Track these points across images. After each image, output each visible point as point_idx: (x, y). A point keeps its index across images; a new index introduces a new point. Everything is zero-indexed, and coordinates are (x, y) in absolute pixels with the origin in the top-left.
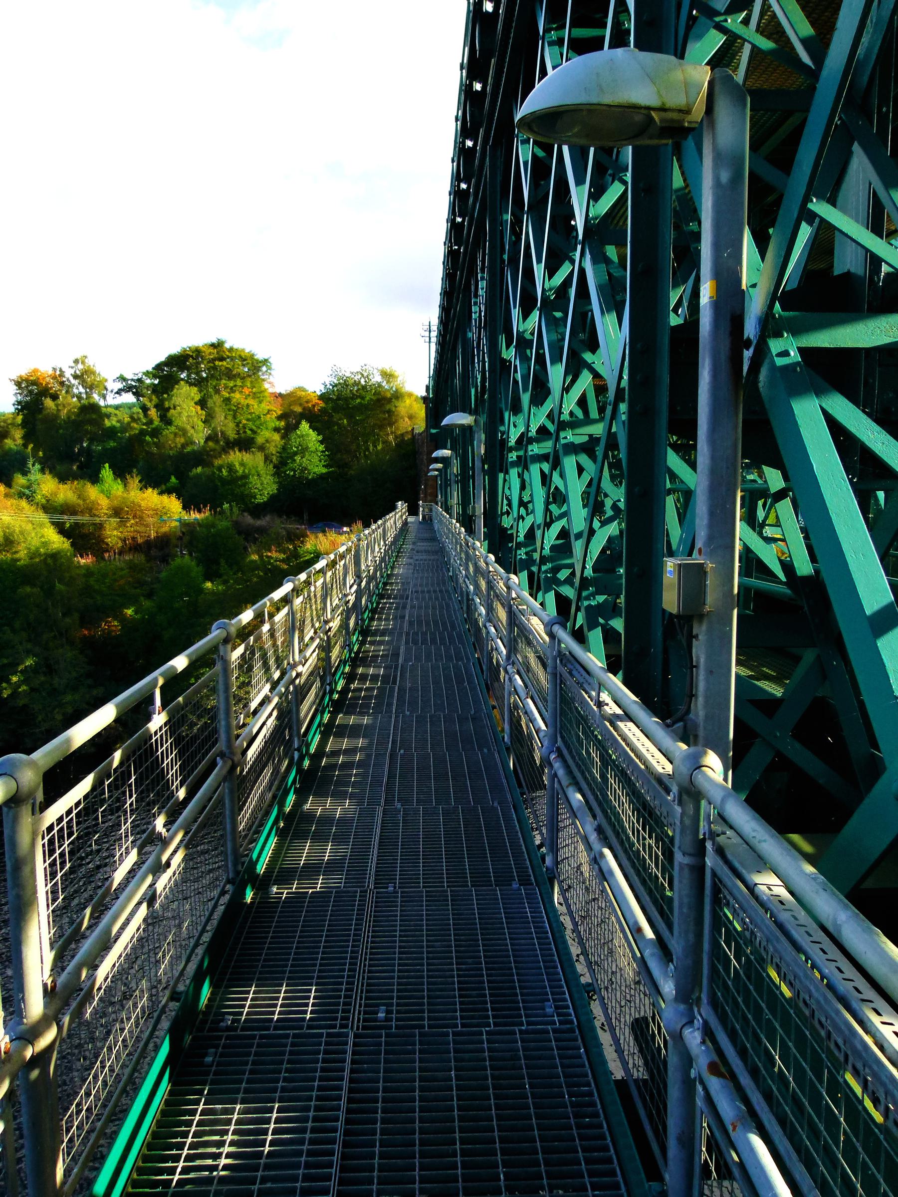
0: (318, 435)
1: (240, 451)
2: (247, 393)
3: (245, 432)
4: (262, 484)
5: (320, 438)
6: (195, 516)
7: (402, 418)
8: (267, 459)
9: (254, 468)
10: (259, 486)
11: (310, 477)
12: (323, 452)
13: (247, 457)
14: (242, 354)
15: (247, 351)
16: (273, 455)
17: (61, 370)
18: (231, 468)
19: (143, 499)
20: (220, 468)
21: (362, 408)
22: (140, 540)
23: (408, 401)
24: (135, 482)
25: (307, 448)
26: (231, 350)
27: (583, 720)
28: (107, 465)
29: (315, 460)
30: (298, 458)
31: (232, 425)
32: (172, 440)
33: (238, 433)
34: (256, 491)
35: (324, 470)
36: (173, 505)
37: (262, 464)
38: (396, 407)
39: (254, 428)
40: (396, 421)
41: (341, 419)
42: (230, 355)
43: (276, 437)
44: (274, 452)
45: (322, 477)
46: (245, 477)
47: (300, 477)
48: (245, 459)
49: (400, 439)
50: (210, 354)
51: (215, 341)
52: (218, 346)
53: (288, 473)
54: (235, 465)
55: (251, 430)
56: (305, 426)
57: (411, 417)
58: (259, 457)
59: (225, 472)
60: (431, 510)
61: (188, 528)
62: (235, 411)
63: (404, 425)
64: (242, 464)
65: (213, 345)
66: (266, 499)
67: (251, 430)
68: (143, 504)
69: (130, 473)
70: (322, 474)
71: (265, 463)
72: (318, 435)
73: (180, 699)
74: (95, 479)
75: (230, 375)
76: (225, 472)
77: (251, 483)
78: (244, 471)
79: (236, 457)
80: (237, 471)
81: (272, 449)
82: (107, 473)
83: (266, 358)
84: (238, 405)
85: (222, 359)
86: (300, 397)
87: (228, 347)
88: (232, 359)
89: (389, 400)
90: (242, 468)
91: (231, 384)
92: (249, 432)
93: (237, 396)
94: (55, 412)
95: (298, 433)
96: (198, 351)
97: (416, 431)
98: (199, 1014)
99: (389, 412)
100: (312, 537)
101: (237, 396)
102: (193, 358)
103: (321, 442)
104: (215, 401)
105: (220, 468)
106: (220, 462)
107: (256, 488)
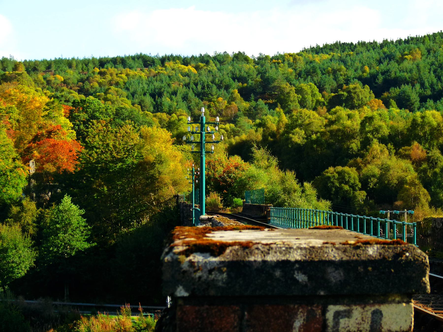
0: (80, 209)
5: (83, 212)
8: (24, 230)
9: (11, 240)
10: (17, 260)
12: (85, 226)
16: (29, 225)
21: (122, 173)
23: (172, 165)
25: (70, 224)
27: (28, 181)
30: (61, 235)
34: (14, 265)
35: (86, 246)
38: (160, 173)
40: (160, 188)
41: (100, 186)
44: (30, 222)
47: (63, 254)
53: (51, 249)
57: (175, 183)
58: (17, 228)
66: (23, 274)
70: (86, 250)
71: (23, 235)
72: (80, 209)
77: (10, 256)
89: (152, 165)
98: (320, 175)
100: (85, 320)
103: (83, 216)
107: (13, 262)
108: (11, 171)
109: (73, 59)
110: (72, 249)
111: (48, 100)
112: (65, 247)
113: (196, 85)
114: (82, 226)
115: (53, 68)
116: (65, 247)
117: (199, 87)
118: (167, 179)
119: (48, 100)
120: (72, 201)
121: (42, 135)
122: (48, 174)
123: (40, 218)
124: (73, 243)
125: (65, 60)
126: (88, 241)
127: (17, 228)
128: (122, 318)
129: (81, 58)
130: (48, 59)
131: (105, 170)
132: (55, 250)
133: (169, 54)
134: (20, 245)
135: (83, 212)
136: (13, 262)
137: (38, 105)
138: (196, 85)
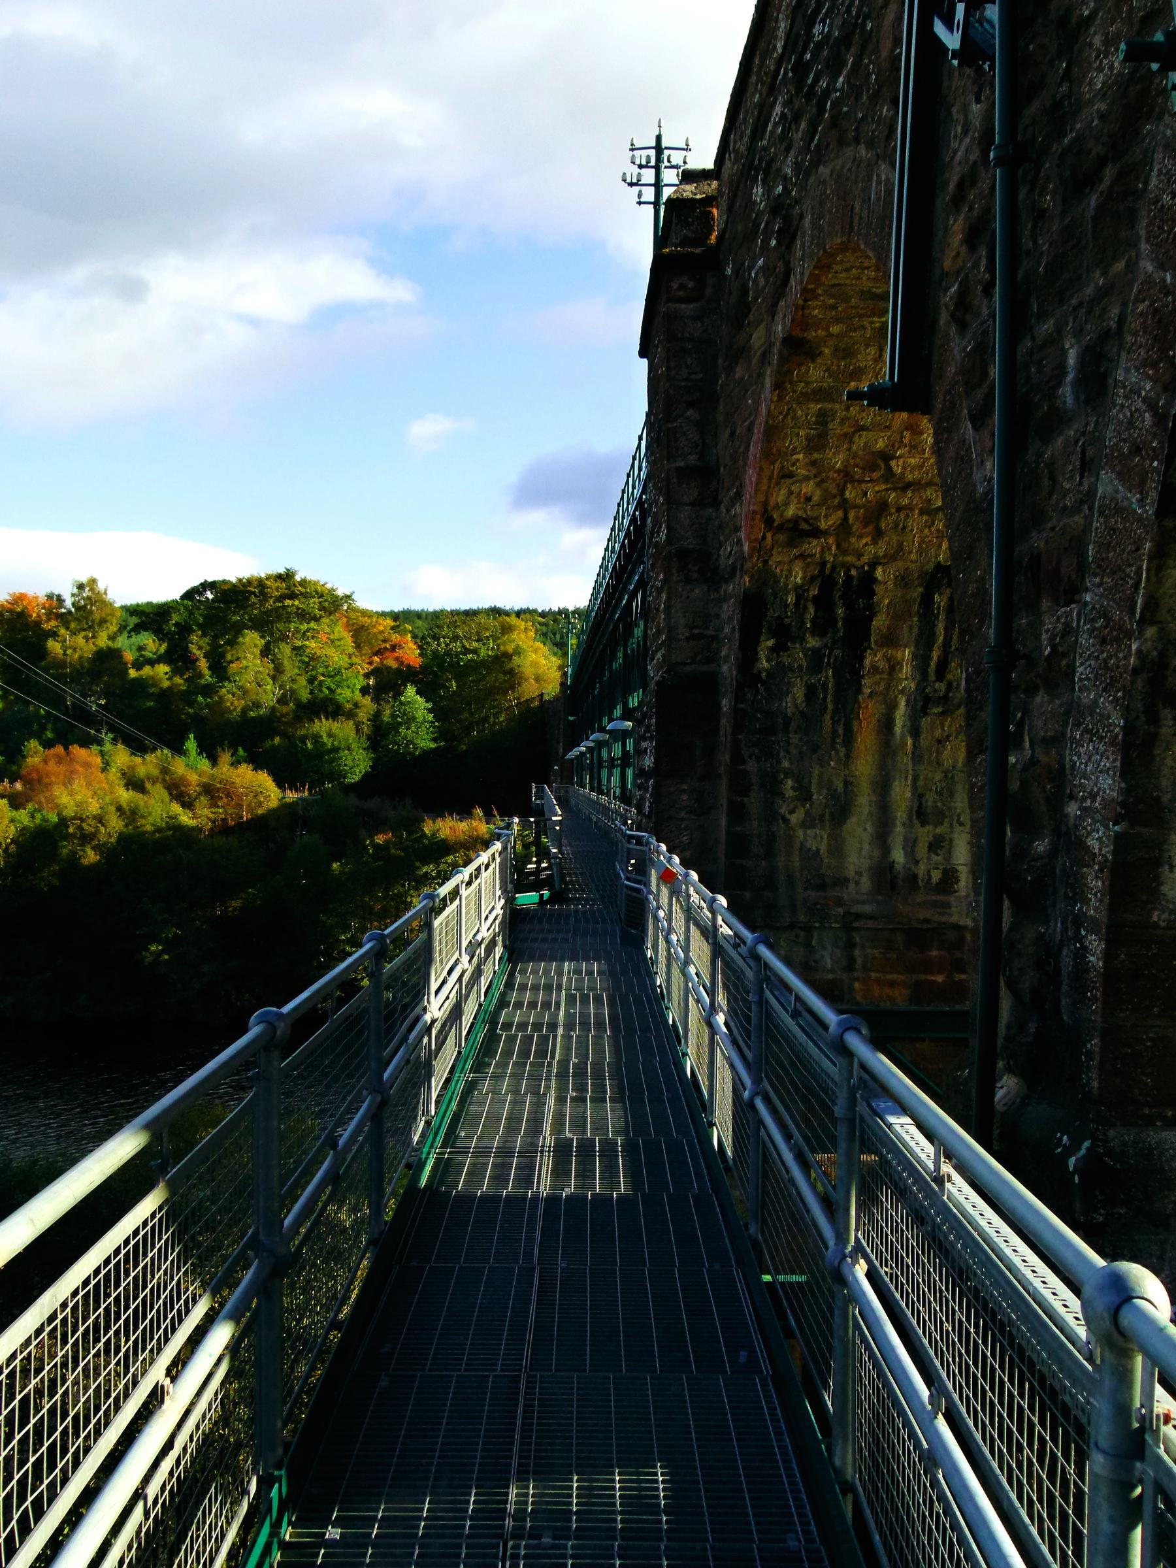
0: (426, 702)
1: (327, 719)
2: (324, 640)
3: (321, 691)
4: (353, 760)
6: (292, 796)
7: (526, 680)
8: (358, 730)
10: (349, 762)
11: (276, 724)
13: (335, 726)
14: (319, 589)
15: (329, 586)
17: (59, 596)
18: (316, 738)
19: (238, 776)
20: (303, 739)
21: (473, 667)
22: (231, 823)
24: (225, 758)
25: (414, 718)
26: (304, 582)
28: (192, 736)
29: (423, 732)
30: (402, 730)
31: (303, 681)
32: (232, 700)
33: (311, 693)
35: (433, 745)
36: (265, 780)
37: (353, 734)
39: (333, 686)
40: (519, 684)
42: (303, 590)
43: (367, 701)
45: (426, 753)
46: (336, 750)
48: (334, 728)
49: (525, 705)
50: (277, 589)
51: (282, 571)
52: (286, 577)
54: (321, 737)
55: (329, 688)
56: (411, 691)
57: (538, 679)
58: (350, 725)
59: (309, 745)
60: (567, 792)
61: (286, 808)
62: (309, 663)
63: (529, 690)
64: (330, 735)
65: (279, 577)
67: (329, 688)
68: (238, 780)
69: (222, 745)
72: (426, 702)
73: (840, 611)
74: (178, 749)
75: (303, 616)
76: (309, 745)
78: (333, 744)
79: (323, 726)
80: (324, 744)
81: (363, 716)
82: (191, 745)
83: (348, 594)
84: (313, 658)
85: (292, 596)
86: (363, 626)
87: (299, 580)
88: (306, 595)
90: (331, 740)
91: (304, 627)
92: (327, 692)
93: (312, 644)
94: (61, 656)
95: (403, 699)
96: (261, 583)
97: (546, 698)
99: (511, 672)
101: (312, 644)
102: (255, 595)
103: (430, 711)
104: (285, 650)
105: (303, 739)
106: (303, 732)
107: (346, 765)
108: (346, 669)
109: (423, 610)
110: (415, 748)
111: (393, 624)
112: (407, 745)
113: (555, 634)
114: (428, 722)
115: (401, 619)
116: (407, 745)
117: (558, 637)
118: (528, 672)
119: (393, 624)
120: (418, 692)
121: (385, 648)
122: (389, 668)
123: (377, 715)
124: (418, 741)
125: (414, 611)
126: (434, 740)
127: (350, 725)
128: (475, 824)
129: (431, 609)
130: (396, 611)
131: (454, 665)
132: (396, 747)
133: (524, 607)
134: (354, 745)
135: (429, 705)
136: (346, 765)
137: (382, 628)
138: (555, 634)
